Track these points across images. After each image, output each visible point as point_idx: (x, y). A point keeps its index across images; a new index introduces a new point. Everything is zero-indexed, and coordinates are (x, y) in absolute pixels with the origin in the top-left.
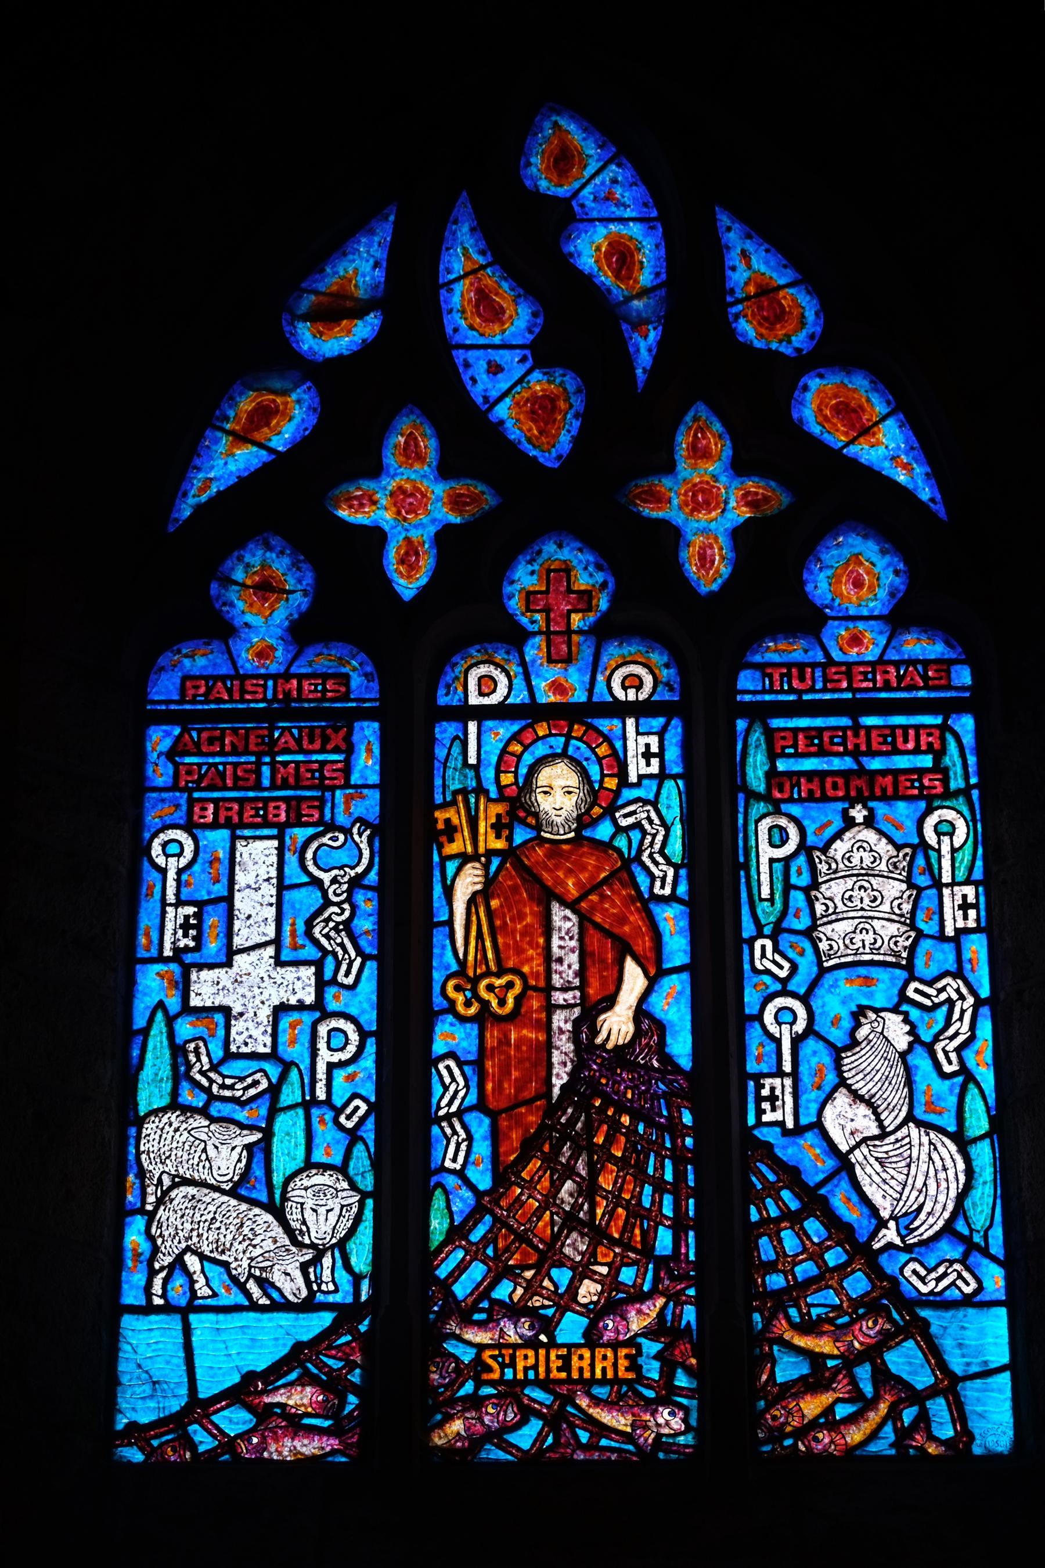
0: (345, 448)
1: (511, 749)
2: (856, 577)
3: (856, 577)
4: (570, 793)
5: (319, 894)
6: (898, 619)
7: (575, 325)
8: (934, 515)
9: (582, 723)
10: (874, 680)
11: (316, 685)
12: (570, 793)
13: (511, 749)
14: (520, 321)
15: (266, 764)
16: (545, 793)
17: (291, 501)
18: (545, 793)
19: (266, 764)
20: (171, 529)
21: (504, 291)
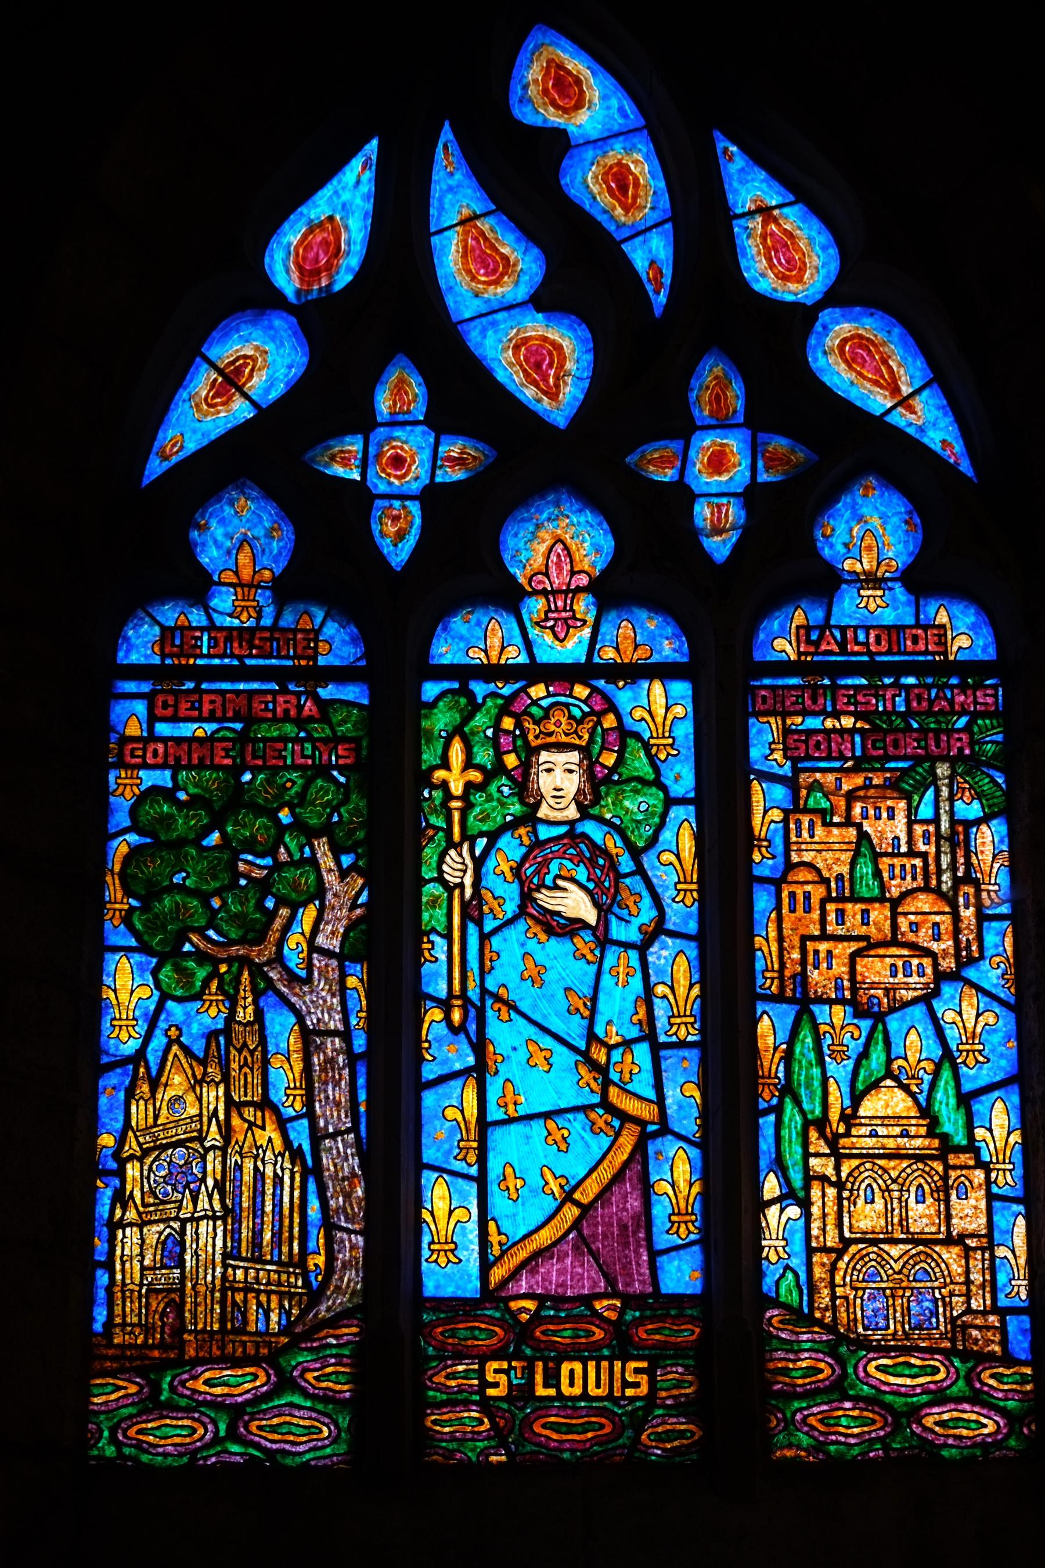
0: (334, 397)
1: (611, 717)
2: (870, 531)
3: (870, 531)
4: (571, 771)
5: (293, 1020)
6: (920, 580)
7: (581, 269)
8: (953, 469)
9: (587, 685)
10: (200, 709)
11: (193, 703)
12: (571, 771)
13: (611, 717)
14: (527, 265)
15: (457, 798)
16: (549, 770)
17: (269, 453)
18: (549, 770)
19: (457, 798)
20: (155, 467)
21: (508, 244)
